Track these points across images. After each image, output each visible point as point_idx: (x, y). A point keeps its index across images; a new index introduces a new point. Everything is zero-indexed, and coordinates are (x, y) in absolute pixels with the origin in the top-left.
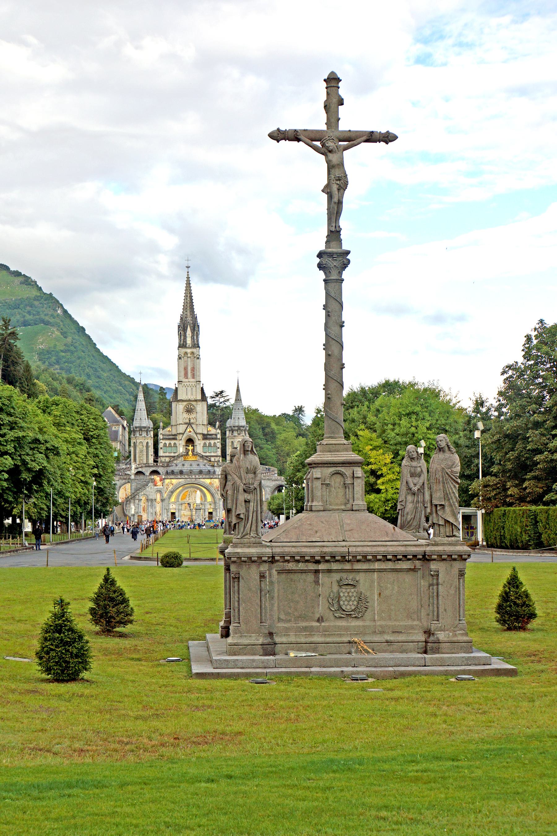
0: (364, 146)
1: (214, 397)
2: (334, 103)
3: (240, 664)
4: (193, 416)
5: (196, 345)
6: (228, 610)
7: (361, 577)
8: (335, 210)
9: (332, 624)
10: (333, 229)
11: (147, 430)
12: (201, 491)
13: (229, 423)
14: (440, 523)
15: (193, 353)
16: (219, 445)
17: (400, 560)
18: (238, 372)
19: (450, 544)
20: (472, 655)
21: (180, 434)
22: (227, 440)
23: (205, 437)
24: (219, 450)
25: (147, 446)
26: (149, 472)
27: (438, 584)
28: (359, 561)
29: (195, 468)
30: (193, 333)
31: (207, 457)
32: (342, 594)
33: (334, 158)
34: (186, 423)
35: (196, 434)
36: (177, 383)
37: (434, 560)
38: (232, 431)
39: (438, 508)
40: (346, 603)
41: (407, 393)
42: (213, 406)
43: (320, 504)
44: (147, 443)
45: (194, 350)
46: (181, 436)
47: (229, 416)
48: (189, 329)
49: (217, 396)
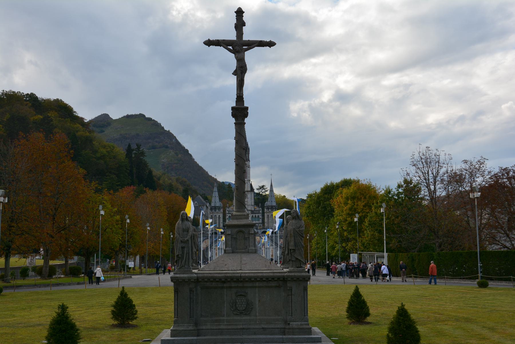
2: (240, 24)
11: (219, 208)
16: (261, 217)
17: (270, 281)
19: (298, 272)
20: (311, 336)
23: (252, 212)
24: (261, 220)
27: (291, 295)
28: (247, 281)
32: (237, 301)
33: (239, 55)
37: (289, 281)
38: (268, 209)
40: (240, 306)
41: (353, 186)
42: (258, 194)
43: (230, 249)
49: (261, 188)
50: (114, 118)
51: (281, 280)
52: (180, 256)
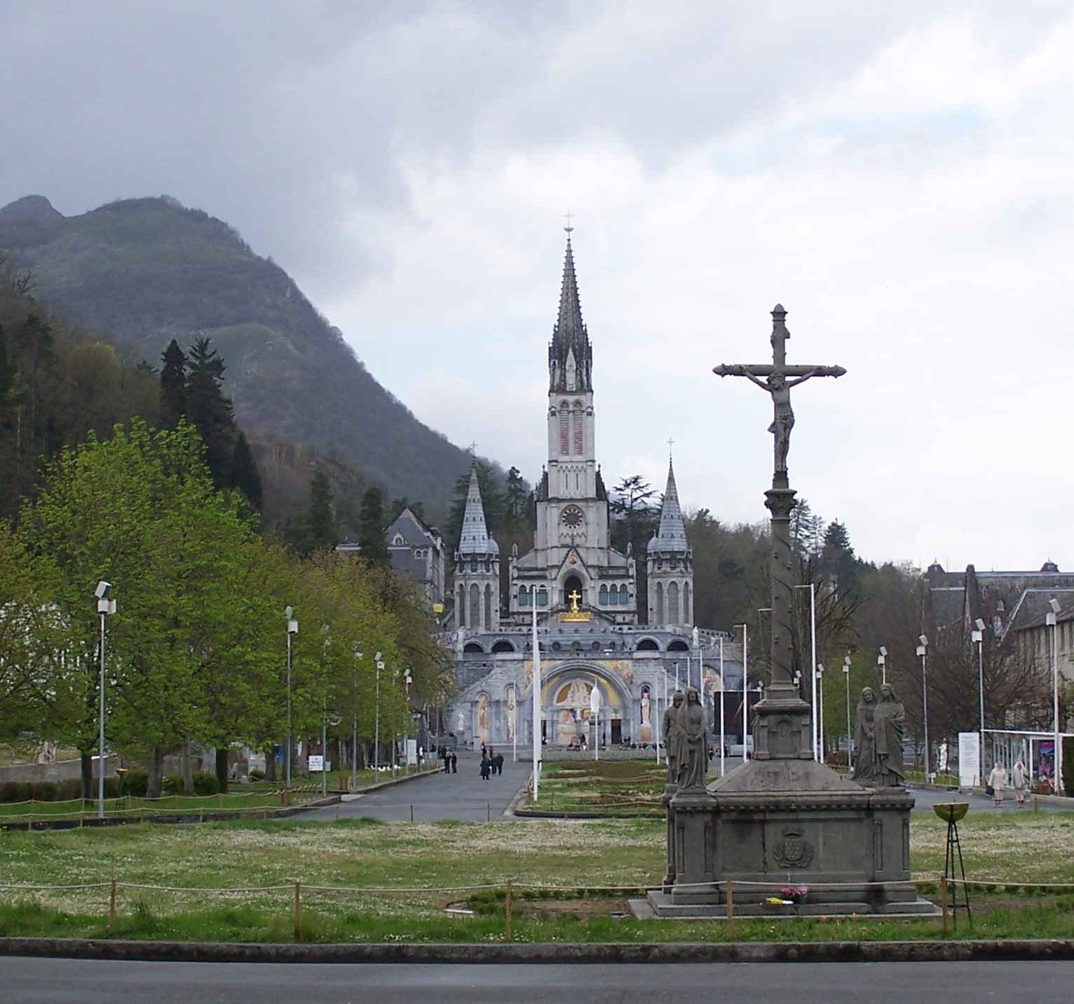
0: (814, 380)
1: (621, 489)
2: (780, 337)
3: (685, 912)
4: (580, 529)
5: (585, 387)
6: (671, 864)
7: (804, 826)
8: (782, 449)
9: (777, 873)
10: (779, 469)
11: (487, 560)
12: (600, 686)
13: (654, 544)
14: (884, 772)
15: (578, 403)
16: (632, 589)
18: (671, 442)
21: (552, 567)
22: (649, 581)
23: (604, 573)
24: (633, 600)
25: (488, 593)
26: (491, 646)
29: (586, 639)
30: (578, 363)
31: (606, 612)
32: (786, 844)
33: (779, 395)
34: (563, 546)
35: (587, 567)
36: (546, 464)
37: (878, 809)
38: (659, 561)
39: (882, 758)
42: (620, 506)
44: (488, 586)
45: (582, 398)
46: (554, 572)
47: (653, 529)
48: (571, 354)
50: (67, 213)
51: (863, 809)
52: (686, 766)
